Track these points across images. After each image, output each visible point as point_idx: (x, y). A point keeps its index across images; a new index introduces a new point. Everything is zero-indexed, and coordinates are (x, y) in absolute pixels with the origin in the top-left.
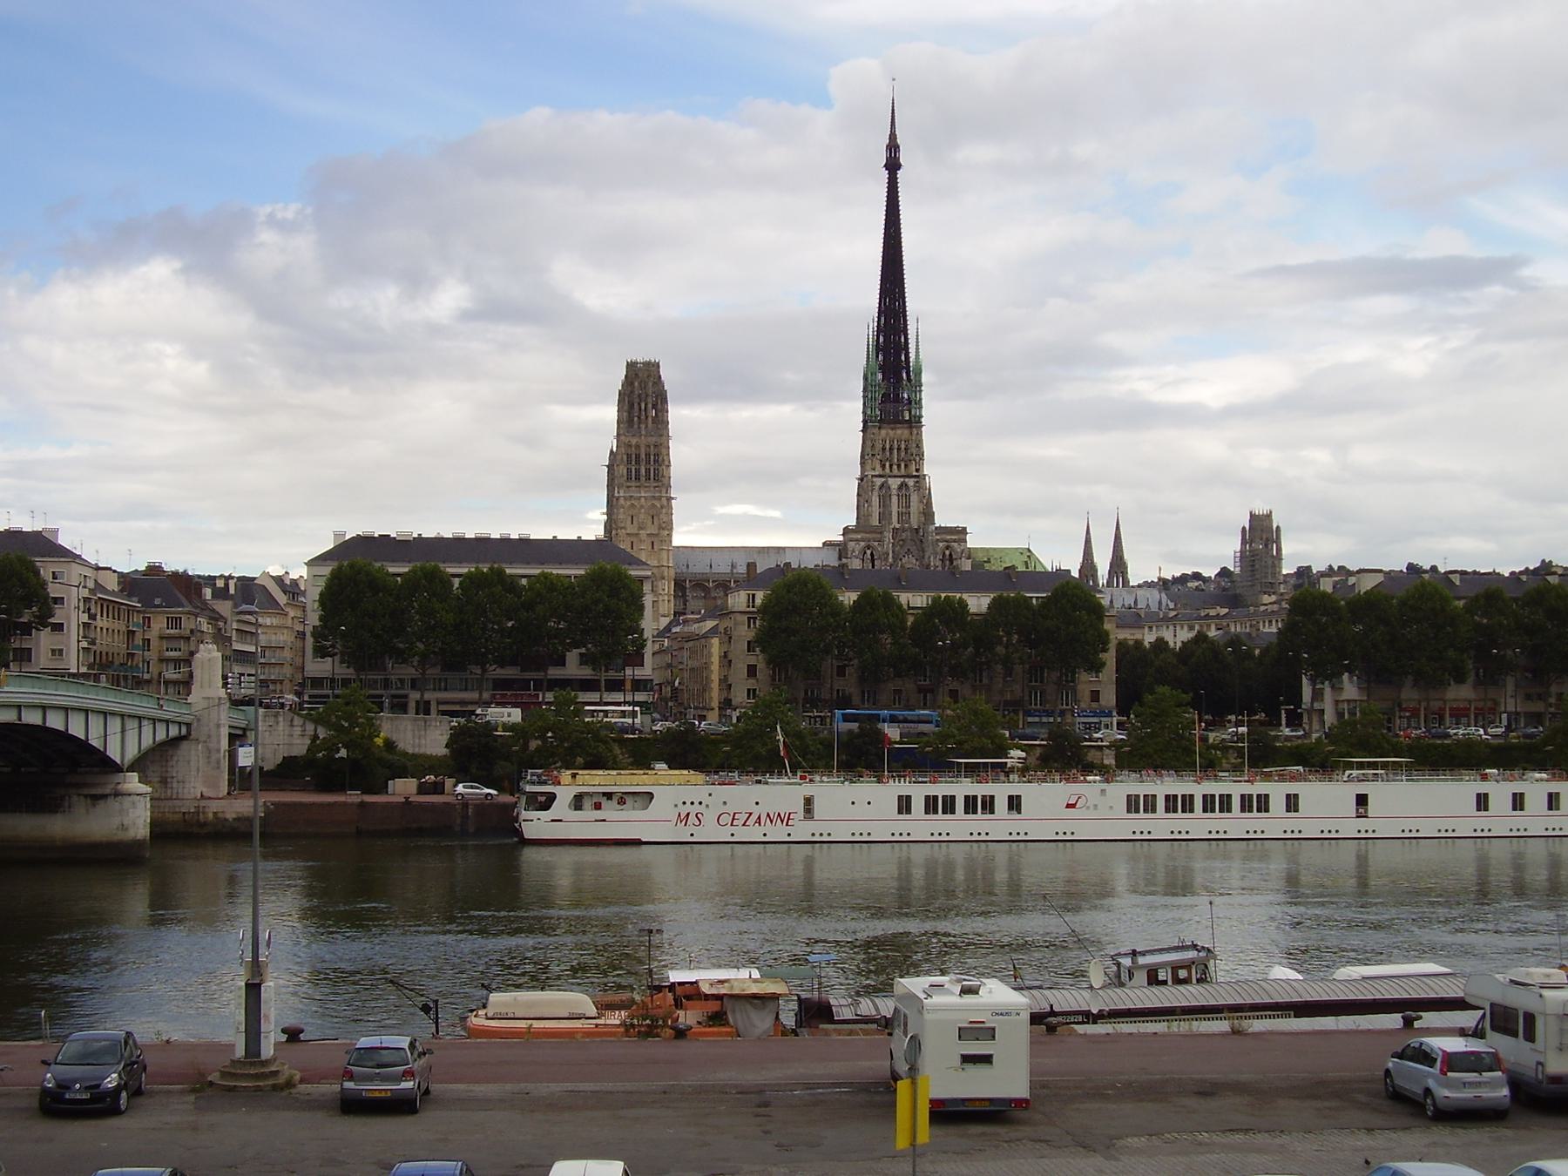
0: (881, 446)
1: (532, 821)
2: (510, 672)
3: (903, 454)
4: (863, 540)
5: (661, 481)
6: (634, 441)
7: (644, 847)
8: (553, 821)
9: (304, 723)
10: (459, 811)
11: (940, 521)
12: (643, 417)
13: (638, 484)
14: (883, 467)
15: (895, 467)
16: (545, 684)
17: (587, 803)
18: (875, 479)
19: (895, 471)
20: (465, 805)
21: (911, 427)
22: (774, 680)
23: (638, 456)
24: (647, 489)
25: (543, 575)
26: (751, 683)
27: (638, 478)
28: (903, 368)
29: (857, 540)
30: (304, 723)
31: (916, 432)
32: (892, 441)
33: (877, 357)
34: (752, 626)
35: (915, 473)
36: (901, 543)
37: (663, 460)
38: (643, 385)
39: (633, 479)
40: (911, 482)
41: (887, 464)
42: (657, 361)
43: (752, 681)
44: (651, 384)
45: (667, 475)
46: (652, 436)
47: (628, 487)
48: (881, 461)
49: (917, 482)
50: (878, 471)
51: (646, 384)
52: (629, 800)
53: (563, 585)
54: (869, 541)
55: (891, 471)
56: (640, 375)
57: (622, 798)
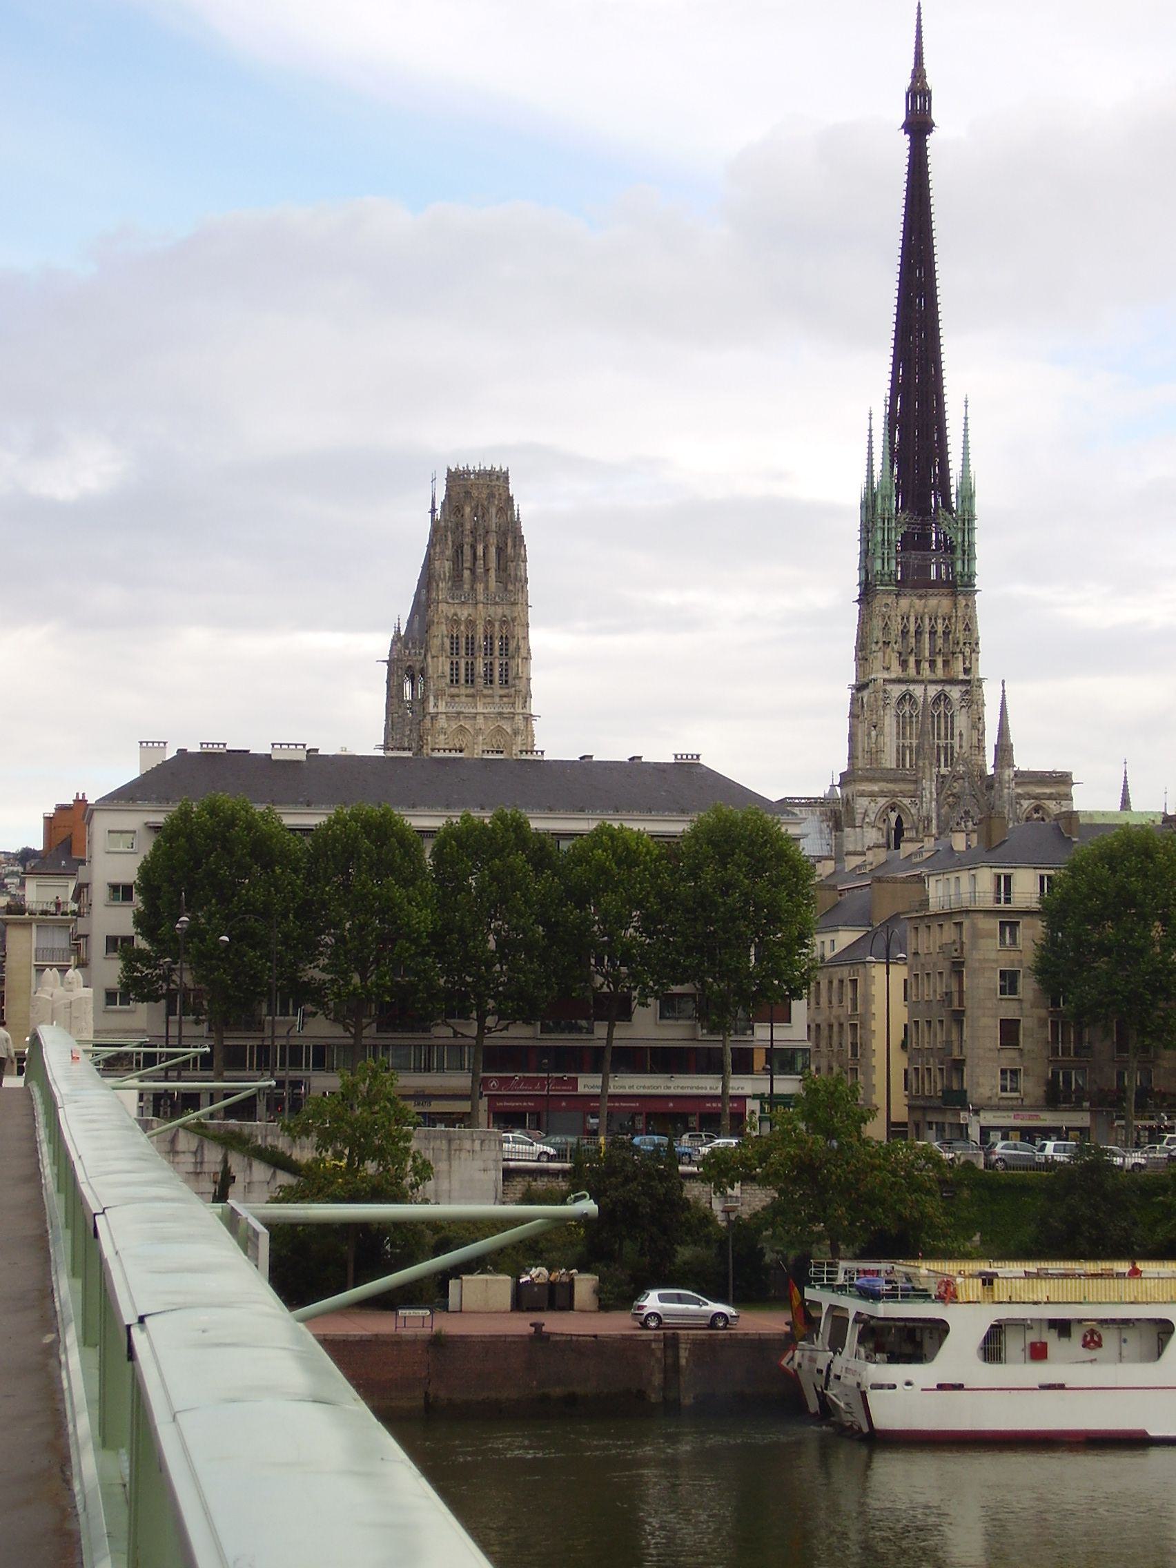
0: (900, 627)
1: (894, 1387)
2: (520, 1034)
3: (940, 642)
4: (882, 794)
5: (514, 686)
6: (464, 613)
7: (1155, 1454)
8: (941, 1387)
9: (201, 1147)
10: (659, 1354)
11: (1024, 761)
12: (480, 571)
13: (470, 691)
14: (904, 664)
15: (925, 665)
16: (608, 1056)
17: (1014, 1345)
18: (889, 687)
19: (926, 672)
20: (671, 1342)
21: (954, 595)
22: (1055, 1051)
23: (471, 641)
24: (488, 700)
25: (603, 835)
26: (1009, 1058)
27: (470, 681)
28: (933, 487)
29: (872, 795)
30: (201, 1147)
31: (964, 603)
32: (919, 618)
33: (892, 468)
34: (1008, 941)
35: (962, 677)
36: (951, 799)
37: (518, 648)
38: (481, 510)
39: (463, 681)
40: (955, 693)
41: (912, 660)
42: (504, 469)
43: (1011, 1053)
44: (493, 511)
45: (524, 675)
46: (496, 603)
47: (452, 696)
48: (900, 654)
49: (967, 692)
50: (896, 672)
51: (486, 511)
52: (1109, 1337)
53: (648, 853)
54: (895, 796)
55: (918, 673)
56: (475, 493)
57: (1092, 1332)
